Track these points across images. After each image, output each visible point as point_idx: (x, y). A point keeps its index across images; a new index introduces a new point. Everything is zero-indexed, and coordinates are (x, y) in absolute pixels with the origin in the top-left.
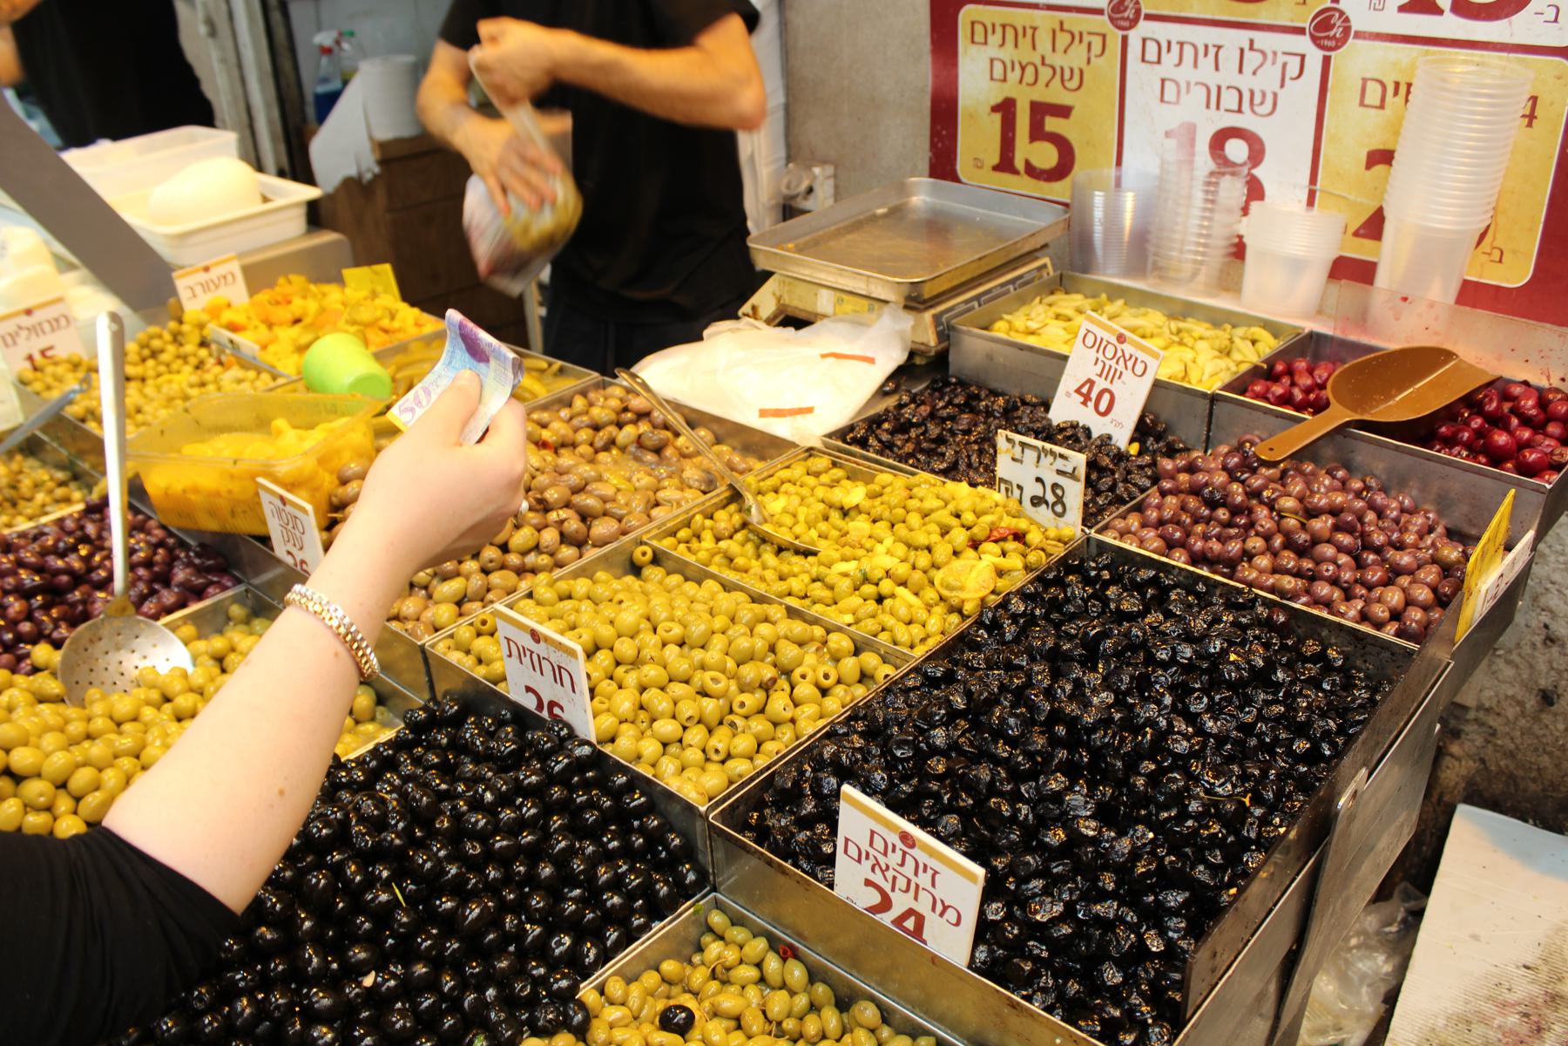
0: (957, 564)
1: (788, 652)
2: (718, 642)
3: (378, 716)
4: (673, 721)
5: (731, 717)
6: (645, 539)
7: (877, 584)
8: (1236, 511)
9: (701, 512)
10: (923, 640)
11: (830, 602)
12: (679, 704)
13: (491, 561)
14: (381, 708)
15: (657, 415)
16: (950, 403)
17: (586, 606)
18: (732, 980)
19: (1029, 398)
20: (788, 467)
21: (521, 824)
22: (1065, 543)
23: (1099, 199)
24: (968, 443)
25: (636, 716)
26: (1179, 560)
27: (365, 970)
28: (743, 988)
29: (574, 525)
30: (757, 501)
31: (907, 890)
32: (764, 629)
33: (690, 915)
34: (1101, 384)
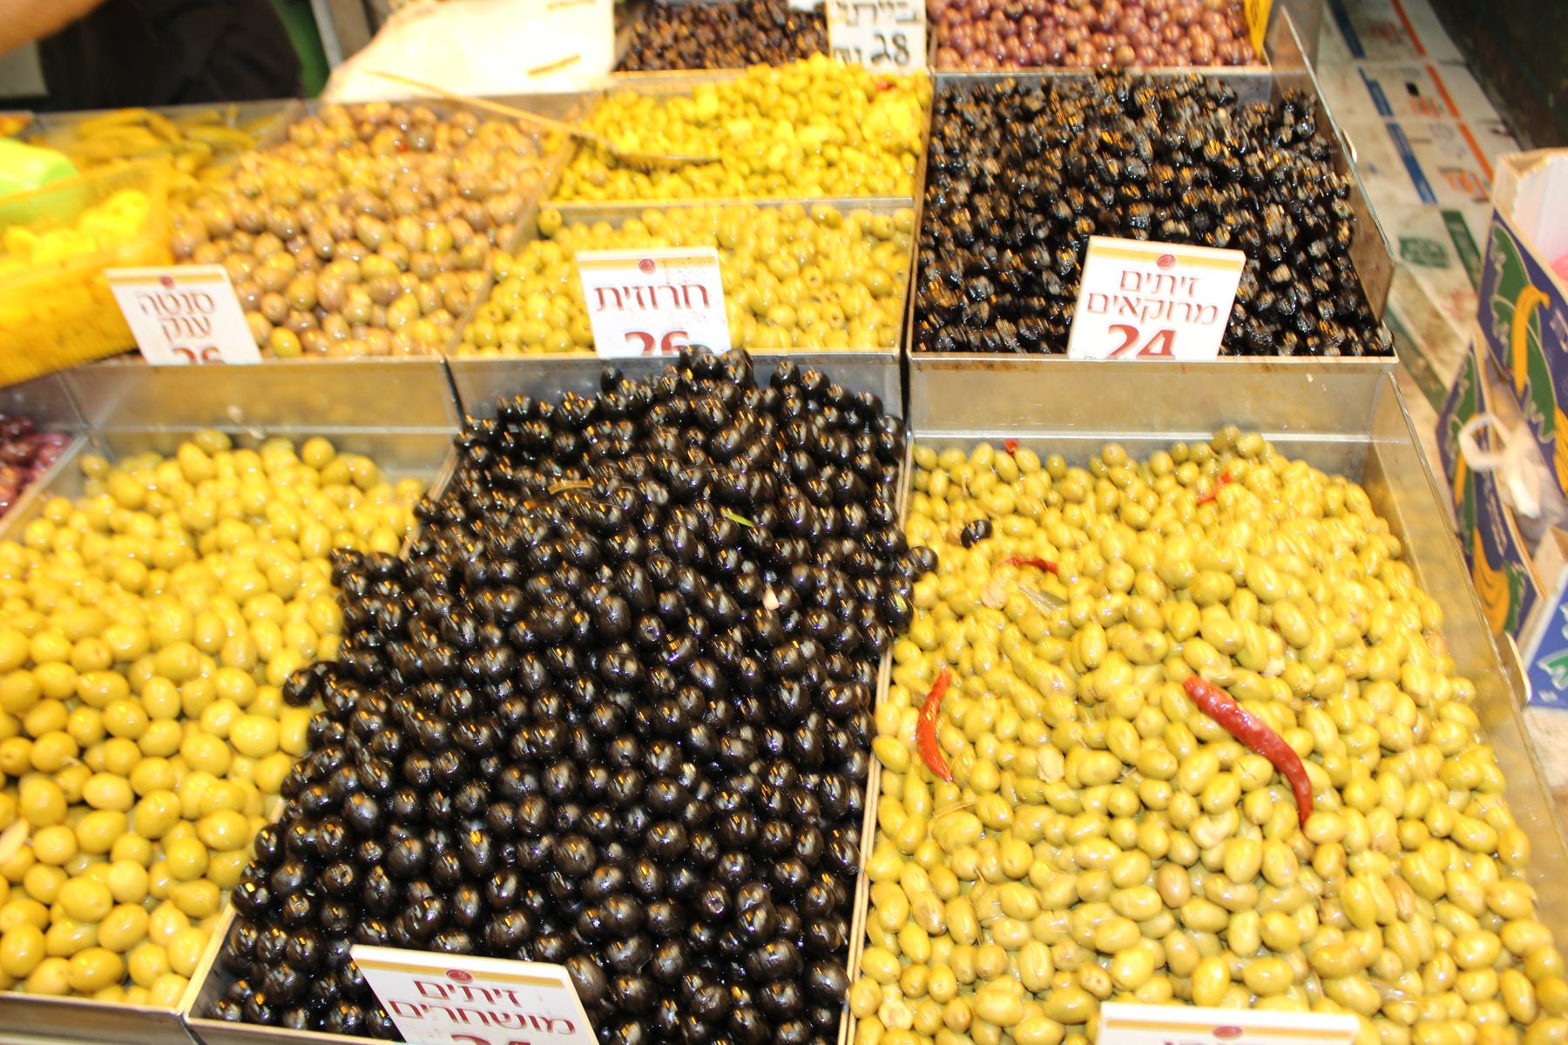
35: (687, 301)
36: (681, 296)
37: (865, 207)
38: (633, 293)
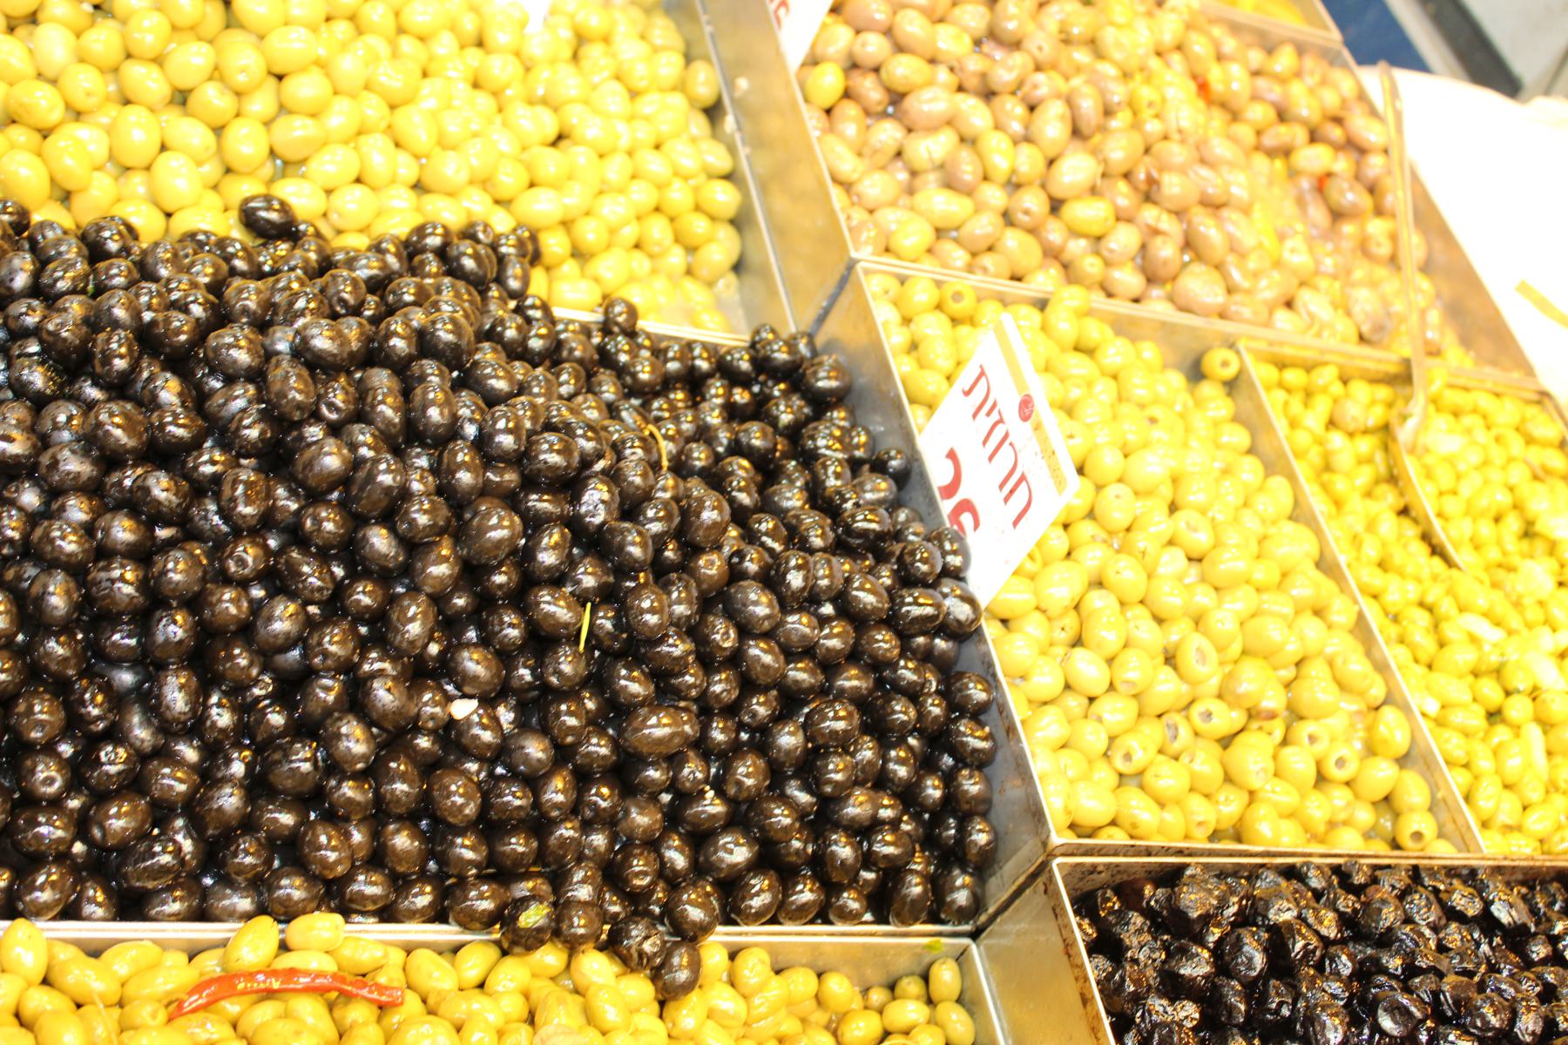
1: (1318, 688)
2: (1241, 601)
3: (721, 284)
4: (1104, 665)
5: (1178, 719)
6: (1242, 344)
7: (1508, 693)
9: (1341, 367)
10: (1508, 829)
11: (1424, 657)
12: (1130, 653)
13: (1027, 212)
14: (732, 277)
15: (1376, 163)
17: (1105, 390)
20: (1497, 395)
21: (808, 651)
29: (1166, 250)
30: (1425, 416)
32: (1310, 624)
33: (917, 946)
35: (1012, 492)
36: (1012, 483)
37: (1433, 788)
38: (995, 417)
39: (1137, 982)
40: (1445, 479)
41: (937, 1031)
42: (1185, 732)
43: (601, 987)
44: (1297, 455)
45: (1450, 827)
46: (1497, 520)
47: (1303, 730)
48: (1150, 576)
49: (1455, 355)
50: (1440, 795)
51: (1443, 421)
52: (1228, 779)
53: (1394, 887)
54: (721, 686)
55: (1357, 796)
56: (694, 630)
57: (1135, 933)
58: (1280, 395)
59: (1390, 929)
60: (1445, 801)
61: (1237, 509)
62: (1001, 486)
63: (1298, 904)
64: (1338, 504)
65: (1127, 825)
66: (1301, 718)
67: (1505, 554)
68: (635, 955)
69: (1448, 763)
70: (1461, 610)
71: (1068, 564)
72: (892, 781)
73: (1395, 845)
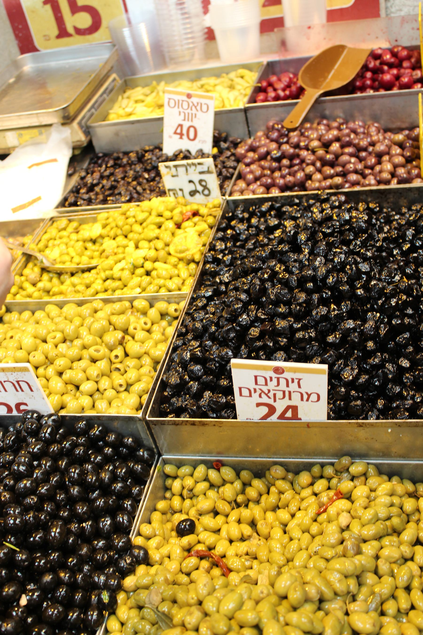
0: (176, 240)
1: (120, 320)
2: (83, 331)
4: (89, 382)
5: (114, 366)
7: (143, 267)
8: (291, 158)
10: (183, 283)
11: (122, 286)
12: (87, 371)
16: (107, 167)
18: (197, 494)
19: (147, 148)
20: (46, 232)
21: (47, 475)
22: (219, 207)
23: (126, 32)
24: (129, 183)
25: (67, 389)
26: (275, 193)
27: (17, 597)
28: (205, 494)
30: (44, 256)
31: (284, 397)
32: (100, 314)
33: (157, 474)
34: (186, 125)
35: (20, 387)
37: (163, 300)
39: (194, 405)
40: (67, 258)
41: (186, 478)
42: (118, 366)
43: (137, 580)
44: (41, 298)
45: (177, 300)
46: (86, 249)
47: (131, 329)
48: (65, 356)
49: (27, 240)
50: (166, 299)
51: (47, 251)
52: (139, 358)
53: (190, 321)
54: (48, 507)
55: (157, 323)
56: (26, 509)
57: (178, 402)
58: (18, 296)
59: (203, 326)
60: (168, 298)
61: (52, 322)
62: (17, 390)
63: (186, 350)
64: (61, 293)
65: (143, 393)
66: (127, 330)
67: (98, 251)
68: (130, 567)
69: (157, 292)
70: (112, 269)
71: (50, 380)
72: (101, 463)
73: (176, 318)
